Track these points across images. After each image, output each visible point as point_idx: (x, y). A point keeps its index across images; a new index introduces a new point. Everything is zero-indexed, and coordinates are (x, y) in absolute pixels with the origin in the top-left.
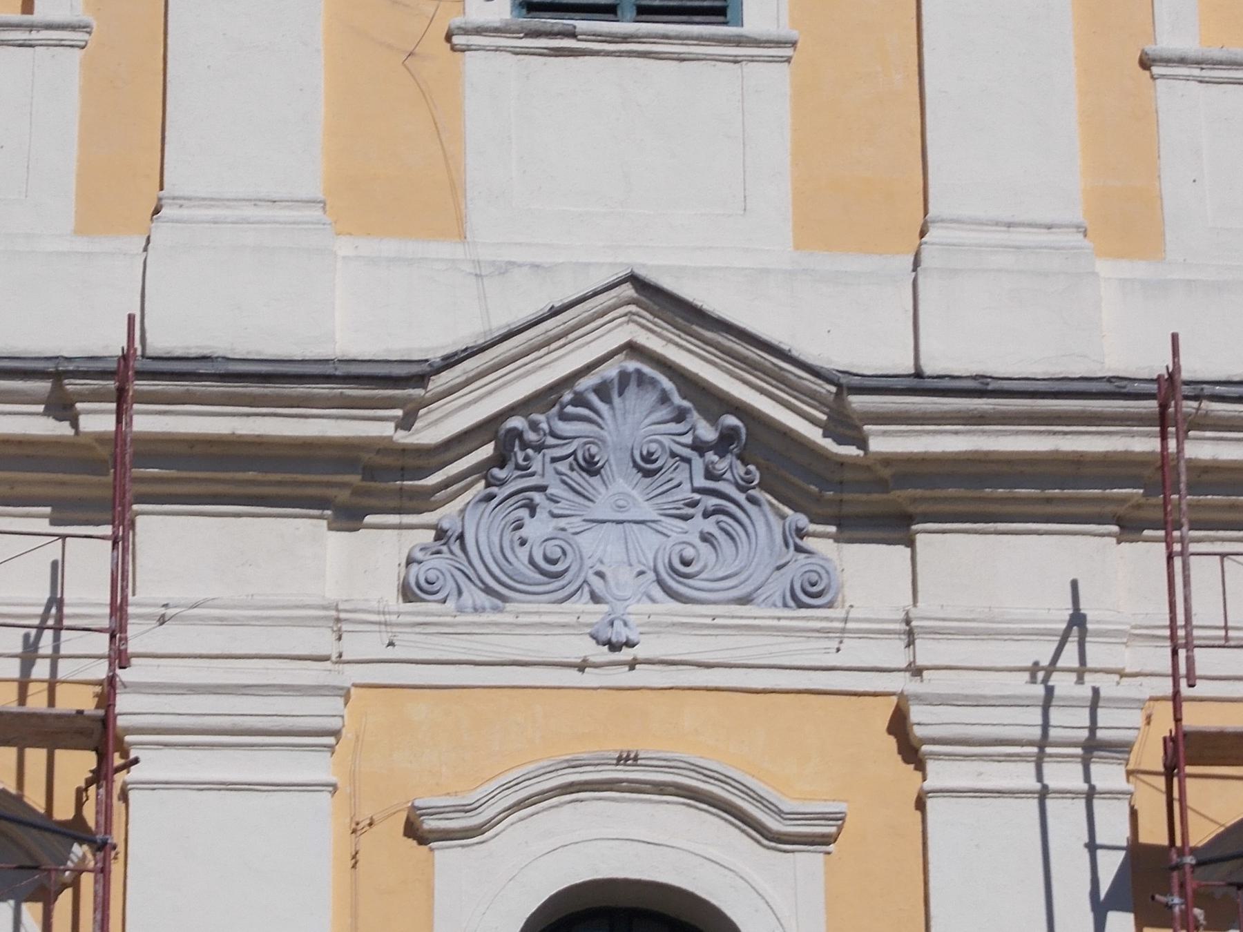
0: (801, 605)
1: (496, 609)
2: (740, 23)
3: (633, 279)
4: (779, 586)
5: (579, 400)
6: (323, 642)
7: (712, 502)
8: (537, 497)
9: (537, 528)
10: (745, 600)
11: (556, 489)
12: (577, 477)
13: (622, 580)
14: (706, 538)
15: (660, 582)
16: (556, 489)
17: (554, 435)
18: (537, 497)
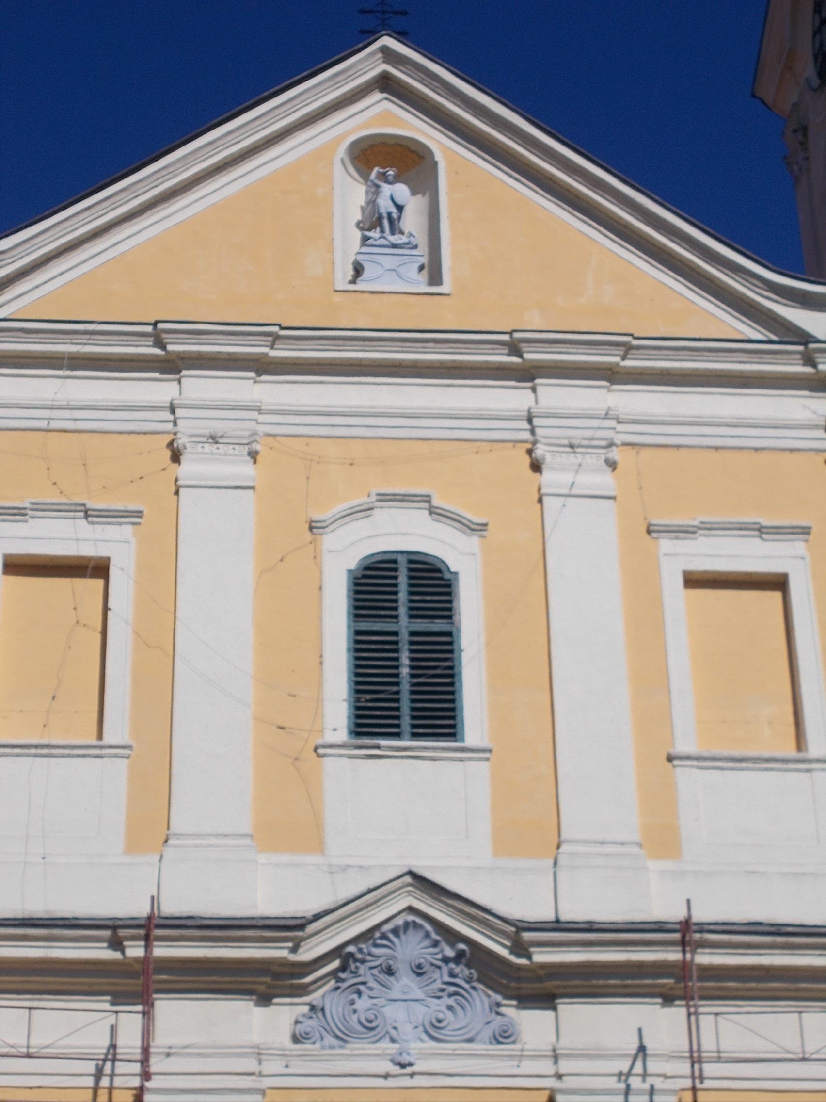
0: (499, 1043)
1: (341, 1047)
2: (463, 740)
3: (411, 873)
4: (488, 1032)
5: (384, 937)
6: (250, 1065)
7: (453, 989)
8: (362, 988)
9: (362, 1004)
10: (470, 1040)
11: (372, 983)
12: (383, 977)
13: (406, 1030)
14: (450, 1008)
15: (426, 1032)
16: (372, 983)
17: (370, 954)
18: (362, 988)
